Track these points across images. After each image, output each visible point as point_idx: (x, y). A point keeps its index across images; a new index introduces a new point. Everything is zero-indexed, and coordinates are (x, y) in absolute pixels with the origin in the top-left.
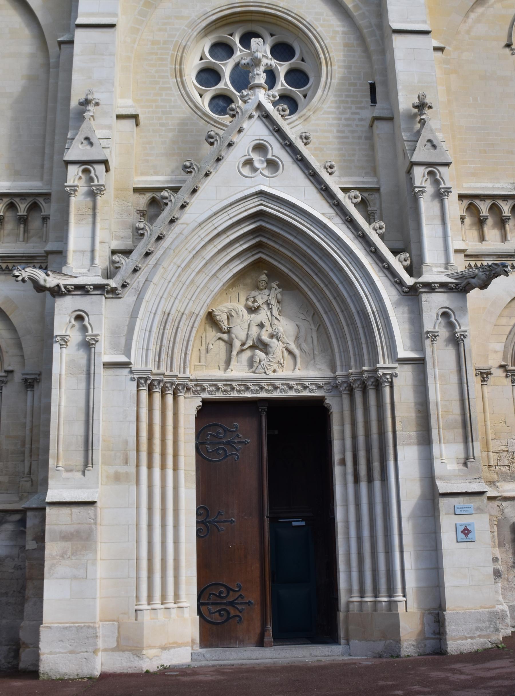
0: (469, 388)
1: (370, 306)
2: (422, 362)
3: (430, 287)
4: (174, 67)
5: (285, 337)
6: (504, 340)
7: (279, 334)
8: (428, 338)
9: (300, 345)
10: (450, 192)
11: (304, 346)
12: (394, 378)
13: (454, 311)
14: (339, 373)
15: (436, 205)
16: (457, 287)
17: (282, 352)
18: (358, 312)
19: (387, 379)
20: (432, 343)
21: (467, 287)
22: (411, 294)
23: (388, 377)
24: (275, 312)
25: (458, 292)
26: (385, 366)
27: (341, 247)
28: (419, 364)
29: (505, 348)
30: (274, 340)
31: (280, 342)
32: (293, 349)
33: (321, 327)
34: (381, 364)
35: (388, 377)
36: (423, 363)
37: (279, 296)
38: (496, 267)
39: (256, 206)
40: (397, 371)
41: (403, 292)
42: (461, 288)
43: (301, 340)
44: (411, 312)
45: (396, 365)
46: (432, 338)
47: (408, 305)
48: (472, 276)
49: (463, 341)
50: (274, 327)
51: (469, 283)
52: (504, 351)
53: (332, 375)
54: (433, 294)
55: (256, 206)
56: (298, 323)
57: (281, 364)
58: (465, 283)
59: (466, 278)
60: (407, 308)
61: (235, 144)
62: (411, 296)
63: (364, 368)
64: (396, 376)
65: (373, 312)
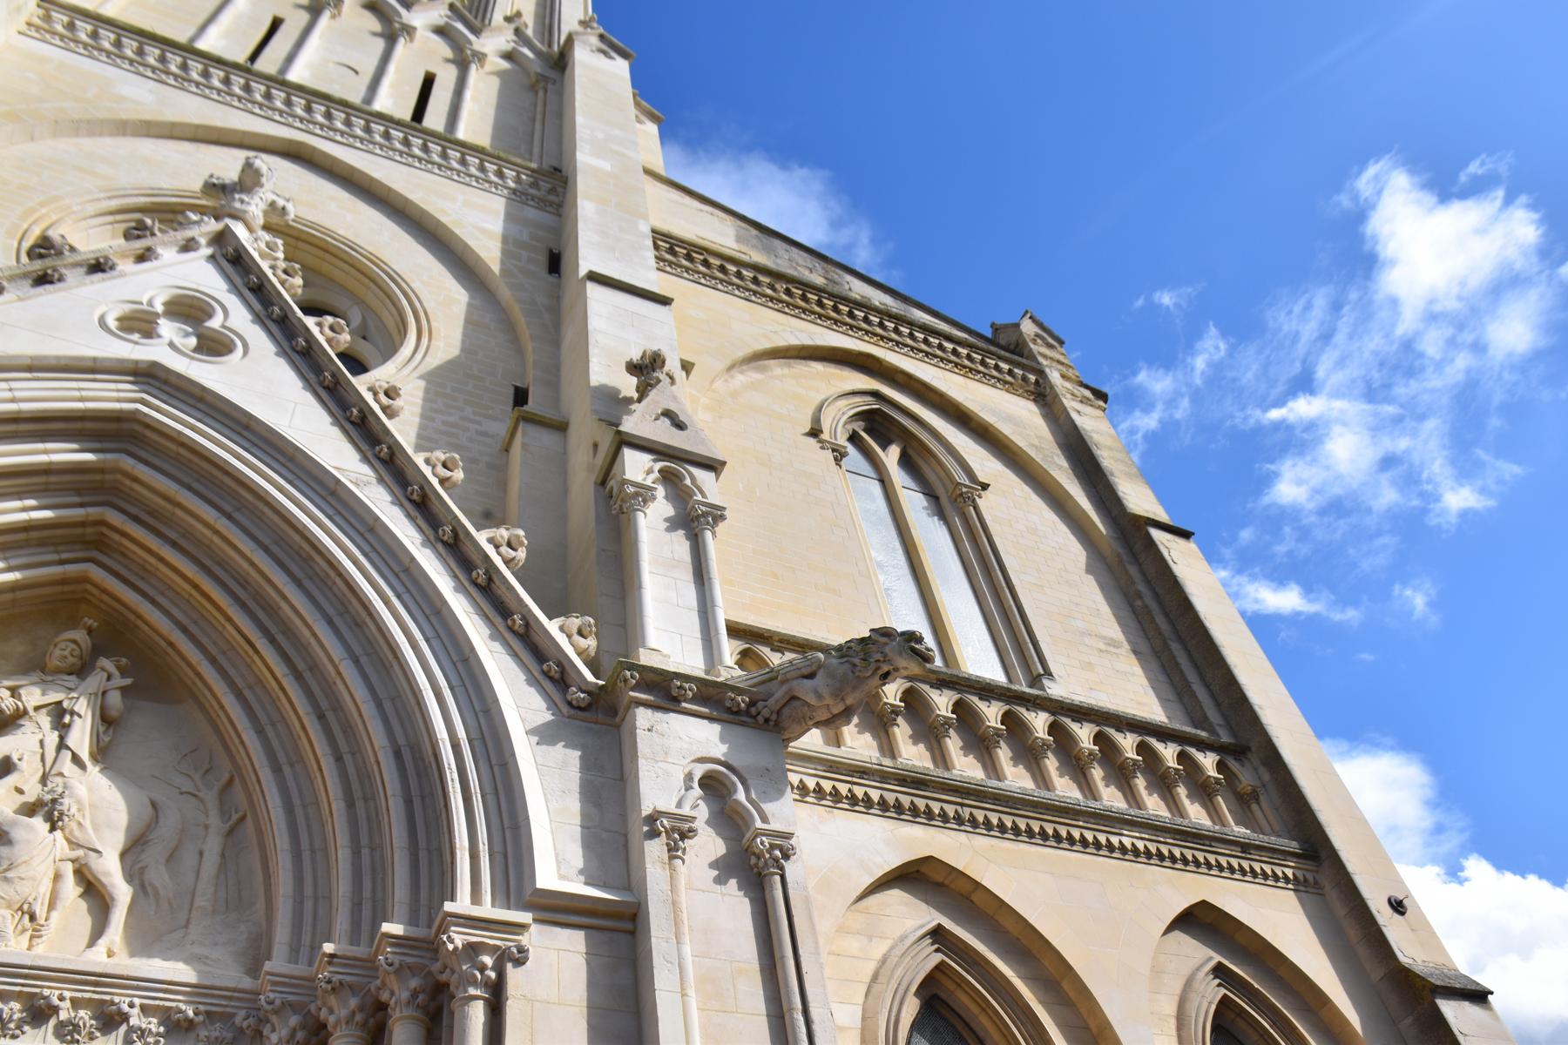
0: (816, 1027)
1: (445, 723)
2: (628, 926)
3: (666, 691)
4: (16, 245)
5: (87, 824)
6: (861, 999)
7: (66, 801)
8: (654, 834)
9: (142, 870)
10: (722, 517)
11: (158, 876)
12: (509, 966)
13: (746, 775)
14: (277, 964)
15: (679, 545)
16: (753, 710)
17: (57, 877)
18: (398, 754)
19: (483, 968)
20: (672, 858)
21: (786, 711)
22: (598, 713)
23: (488, 960)
24: (81, 736)
25: (756, 726)
26: (477, 912)
27: (375, 550)
28: (617, 932)
29: (864, 1019)
30: (39, 823)
31: (58, 833)
32: (108, 874)
33: (239, 827)
34: (461, 904)
35: (488, 960)
36: (633, 933)
37: (115, 699)
38: (884, 640)
39: (119, 400)
40: (524, 939)
41: (570, 704)
42: (766, 713)
43: (153, 855)
44: (589, 766)
45: (524, 917)
46: (668, 836)
47: (583, 748)
48: (806, 671)
49: (782, 868)
50: (56, 783)
51: (794, 698)
52: (863, 1030)
53: (247, 983)
55: (119, 400)
56: (157, 797)
57: (32, 918)
58: (780, 693)
59: (783, 682)
60: (575, 755)
61: (114, 273)
63: (387, 927)
64: (520, 962)
65: (456, 747)
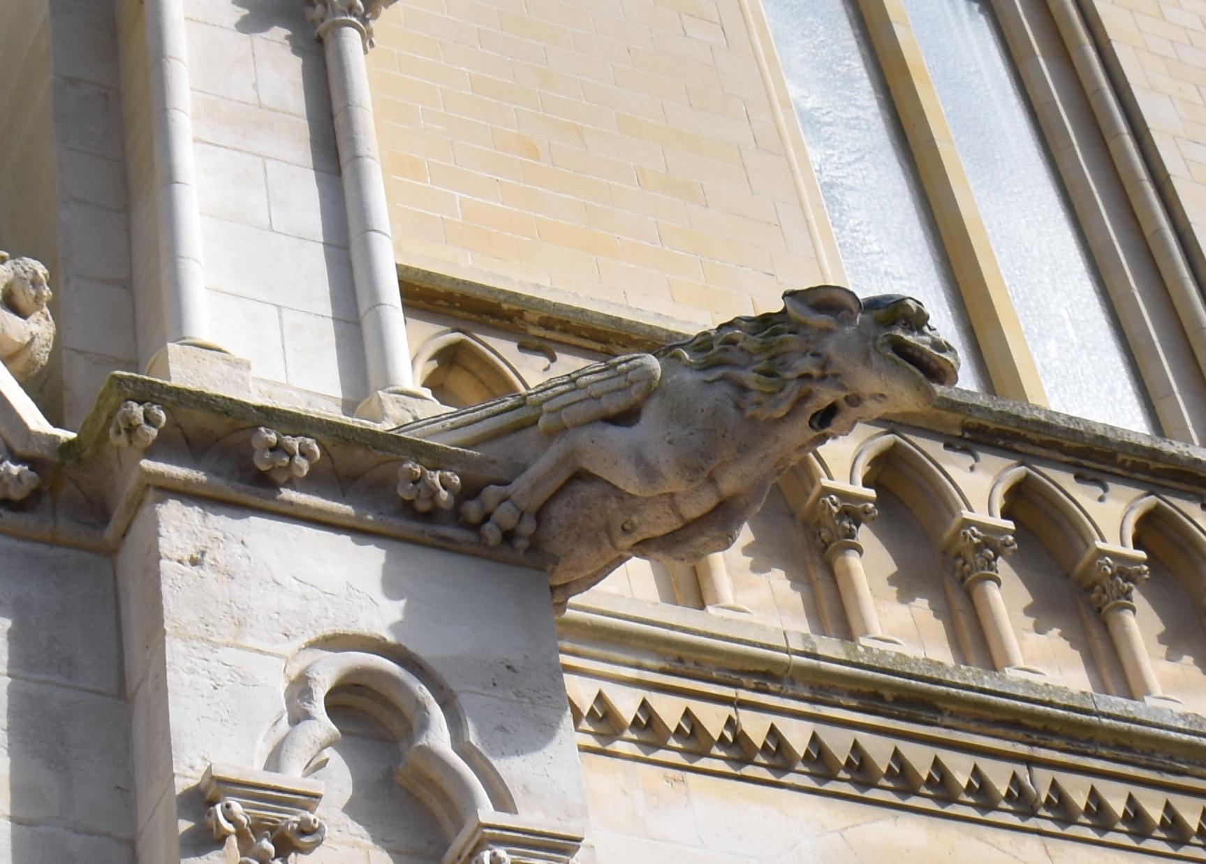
3: (239, 456)
13: (453, 683)
21: (560, 512)
25: (479, 552)
38: (822, 320)
48: (613, 405)
51: (581, 476)
54: (256, 523)
58: (543, 464)
59: (551, 435)
62: (53, 543)
